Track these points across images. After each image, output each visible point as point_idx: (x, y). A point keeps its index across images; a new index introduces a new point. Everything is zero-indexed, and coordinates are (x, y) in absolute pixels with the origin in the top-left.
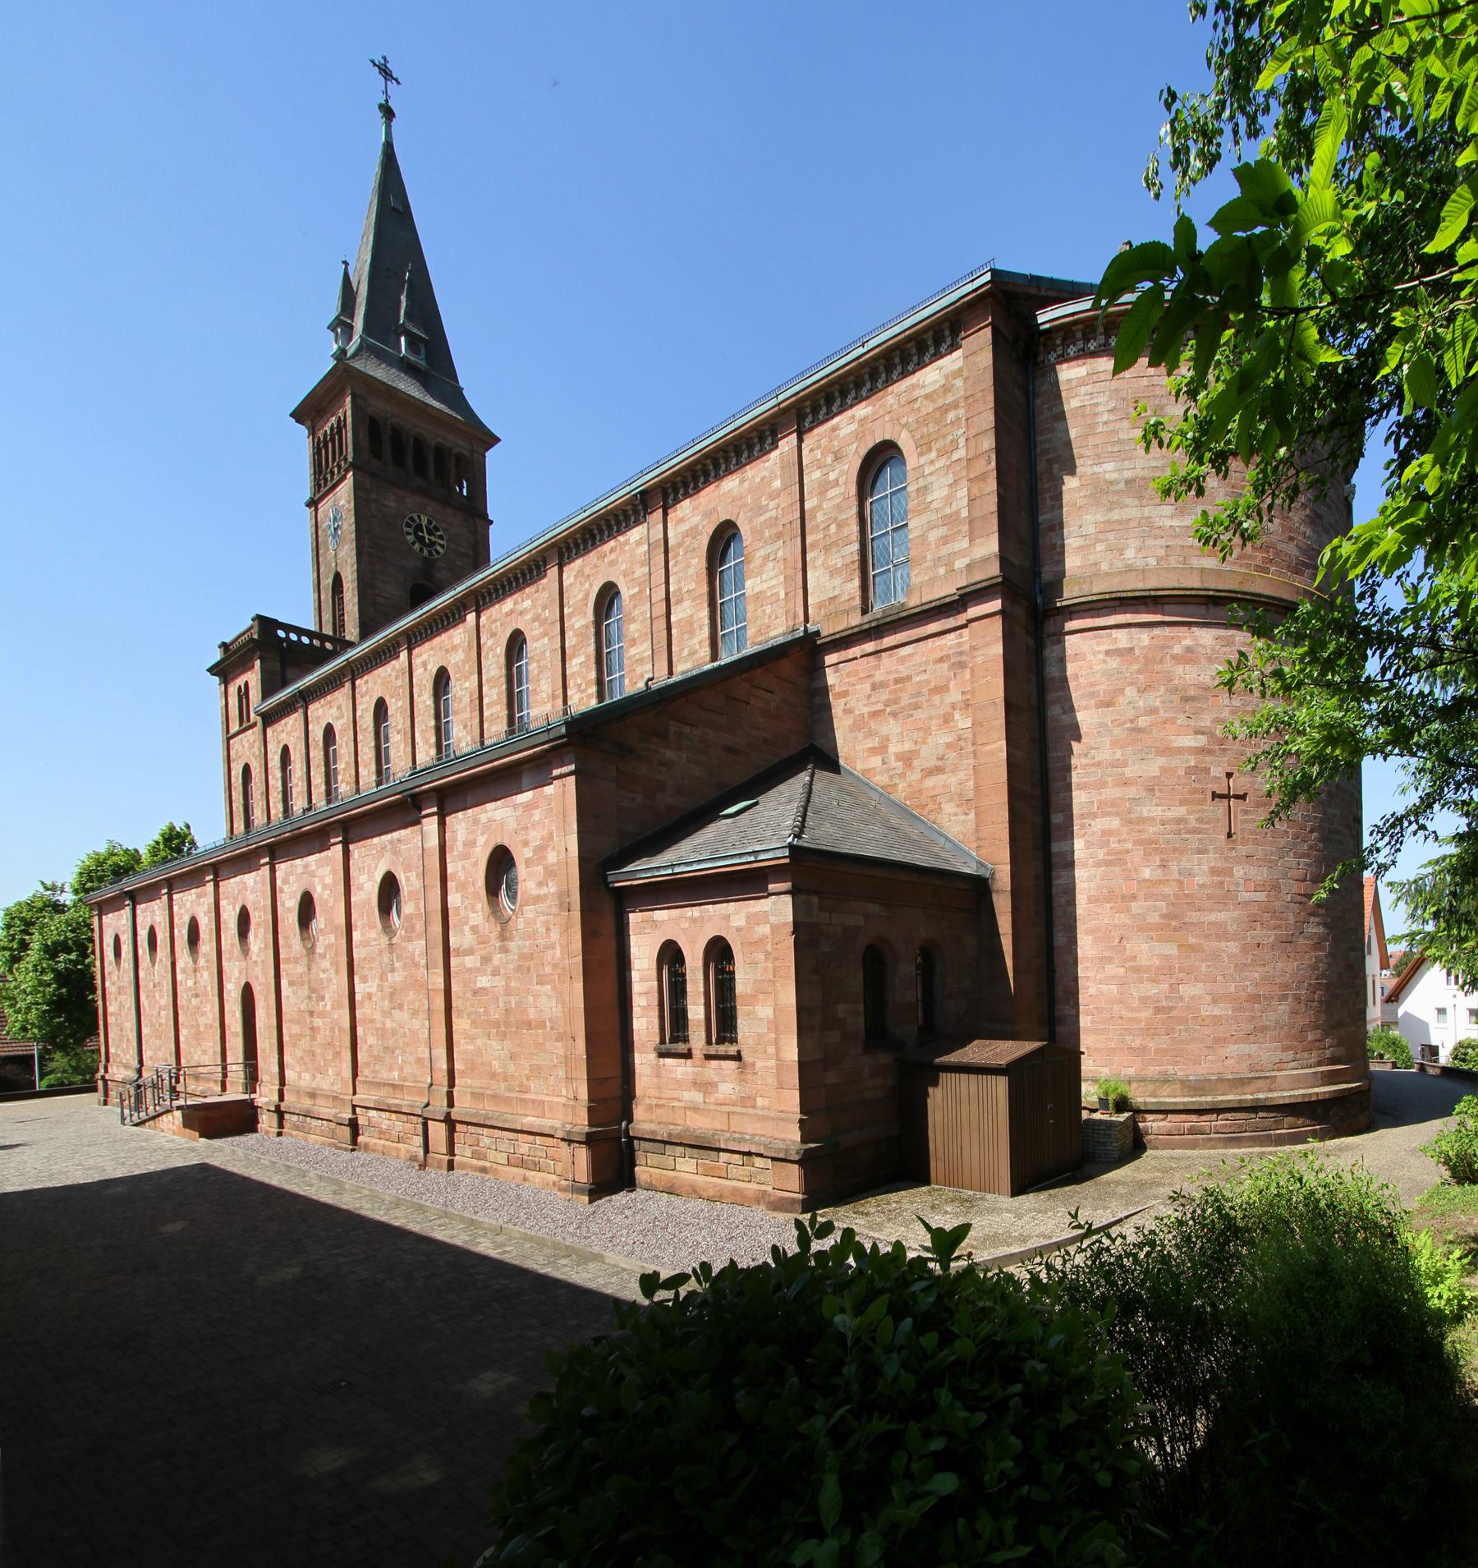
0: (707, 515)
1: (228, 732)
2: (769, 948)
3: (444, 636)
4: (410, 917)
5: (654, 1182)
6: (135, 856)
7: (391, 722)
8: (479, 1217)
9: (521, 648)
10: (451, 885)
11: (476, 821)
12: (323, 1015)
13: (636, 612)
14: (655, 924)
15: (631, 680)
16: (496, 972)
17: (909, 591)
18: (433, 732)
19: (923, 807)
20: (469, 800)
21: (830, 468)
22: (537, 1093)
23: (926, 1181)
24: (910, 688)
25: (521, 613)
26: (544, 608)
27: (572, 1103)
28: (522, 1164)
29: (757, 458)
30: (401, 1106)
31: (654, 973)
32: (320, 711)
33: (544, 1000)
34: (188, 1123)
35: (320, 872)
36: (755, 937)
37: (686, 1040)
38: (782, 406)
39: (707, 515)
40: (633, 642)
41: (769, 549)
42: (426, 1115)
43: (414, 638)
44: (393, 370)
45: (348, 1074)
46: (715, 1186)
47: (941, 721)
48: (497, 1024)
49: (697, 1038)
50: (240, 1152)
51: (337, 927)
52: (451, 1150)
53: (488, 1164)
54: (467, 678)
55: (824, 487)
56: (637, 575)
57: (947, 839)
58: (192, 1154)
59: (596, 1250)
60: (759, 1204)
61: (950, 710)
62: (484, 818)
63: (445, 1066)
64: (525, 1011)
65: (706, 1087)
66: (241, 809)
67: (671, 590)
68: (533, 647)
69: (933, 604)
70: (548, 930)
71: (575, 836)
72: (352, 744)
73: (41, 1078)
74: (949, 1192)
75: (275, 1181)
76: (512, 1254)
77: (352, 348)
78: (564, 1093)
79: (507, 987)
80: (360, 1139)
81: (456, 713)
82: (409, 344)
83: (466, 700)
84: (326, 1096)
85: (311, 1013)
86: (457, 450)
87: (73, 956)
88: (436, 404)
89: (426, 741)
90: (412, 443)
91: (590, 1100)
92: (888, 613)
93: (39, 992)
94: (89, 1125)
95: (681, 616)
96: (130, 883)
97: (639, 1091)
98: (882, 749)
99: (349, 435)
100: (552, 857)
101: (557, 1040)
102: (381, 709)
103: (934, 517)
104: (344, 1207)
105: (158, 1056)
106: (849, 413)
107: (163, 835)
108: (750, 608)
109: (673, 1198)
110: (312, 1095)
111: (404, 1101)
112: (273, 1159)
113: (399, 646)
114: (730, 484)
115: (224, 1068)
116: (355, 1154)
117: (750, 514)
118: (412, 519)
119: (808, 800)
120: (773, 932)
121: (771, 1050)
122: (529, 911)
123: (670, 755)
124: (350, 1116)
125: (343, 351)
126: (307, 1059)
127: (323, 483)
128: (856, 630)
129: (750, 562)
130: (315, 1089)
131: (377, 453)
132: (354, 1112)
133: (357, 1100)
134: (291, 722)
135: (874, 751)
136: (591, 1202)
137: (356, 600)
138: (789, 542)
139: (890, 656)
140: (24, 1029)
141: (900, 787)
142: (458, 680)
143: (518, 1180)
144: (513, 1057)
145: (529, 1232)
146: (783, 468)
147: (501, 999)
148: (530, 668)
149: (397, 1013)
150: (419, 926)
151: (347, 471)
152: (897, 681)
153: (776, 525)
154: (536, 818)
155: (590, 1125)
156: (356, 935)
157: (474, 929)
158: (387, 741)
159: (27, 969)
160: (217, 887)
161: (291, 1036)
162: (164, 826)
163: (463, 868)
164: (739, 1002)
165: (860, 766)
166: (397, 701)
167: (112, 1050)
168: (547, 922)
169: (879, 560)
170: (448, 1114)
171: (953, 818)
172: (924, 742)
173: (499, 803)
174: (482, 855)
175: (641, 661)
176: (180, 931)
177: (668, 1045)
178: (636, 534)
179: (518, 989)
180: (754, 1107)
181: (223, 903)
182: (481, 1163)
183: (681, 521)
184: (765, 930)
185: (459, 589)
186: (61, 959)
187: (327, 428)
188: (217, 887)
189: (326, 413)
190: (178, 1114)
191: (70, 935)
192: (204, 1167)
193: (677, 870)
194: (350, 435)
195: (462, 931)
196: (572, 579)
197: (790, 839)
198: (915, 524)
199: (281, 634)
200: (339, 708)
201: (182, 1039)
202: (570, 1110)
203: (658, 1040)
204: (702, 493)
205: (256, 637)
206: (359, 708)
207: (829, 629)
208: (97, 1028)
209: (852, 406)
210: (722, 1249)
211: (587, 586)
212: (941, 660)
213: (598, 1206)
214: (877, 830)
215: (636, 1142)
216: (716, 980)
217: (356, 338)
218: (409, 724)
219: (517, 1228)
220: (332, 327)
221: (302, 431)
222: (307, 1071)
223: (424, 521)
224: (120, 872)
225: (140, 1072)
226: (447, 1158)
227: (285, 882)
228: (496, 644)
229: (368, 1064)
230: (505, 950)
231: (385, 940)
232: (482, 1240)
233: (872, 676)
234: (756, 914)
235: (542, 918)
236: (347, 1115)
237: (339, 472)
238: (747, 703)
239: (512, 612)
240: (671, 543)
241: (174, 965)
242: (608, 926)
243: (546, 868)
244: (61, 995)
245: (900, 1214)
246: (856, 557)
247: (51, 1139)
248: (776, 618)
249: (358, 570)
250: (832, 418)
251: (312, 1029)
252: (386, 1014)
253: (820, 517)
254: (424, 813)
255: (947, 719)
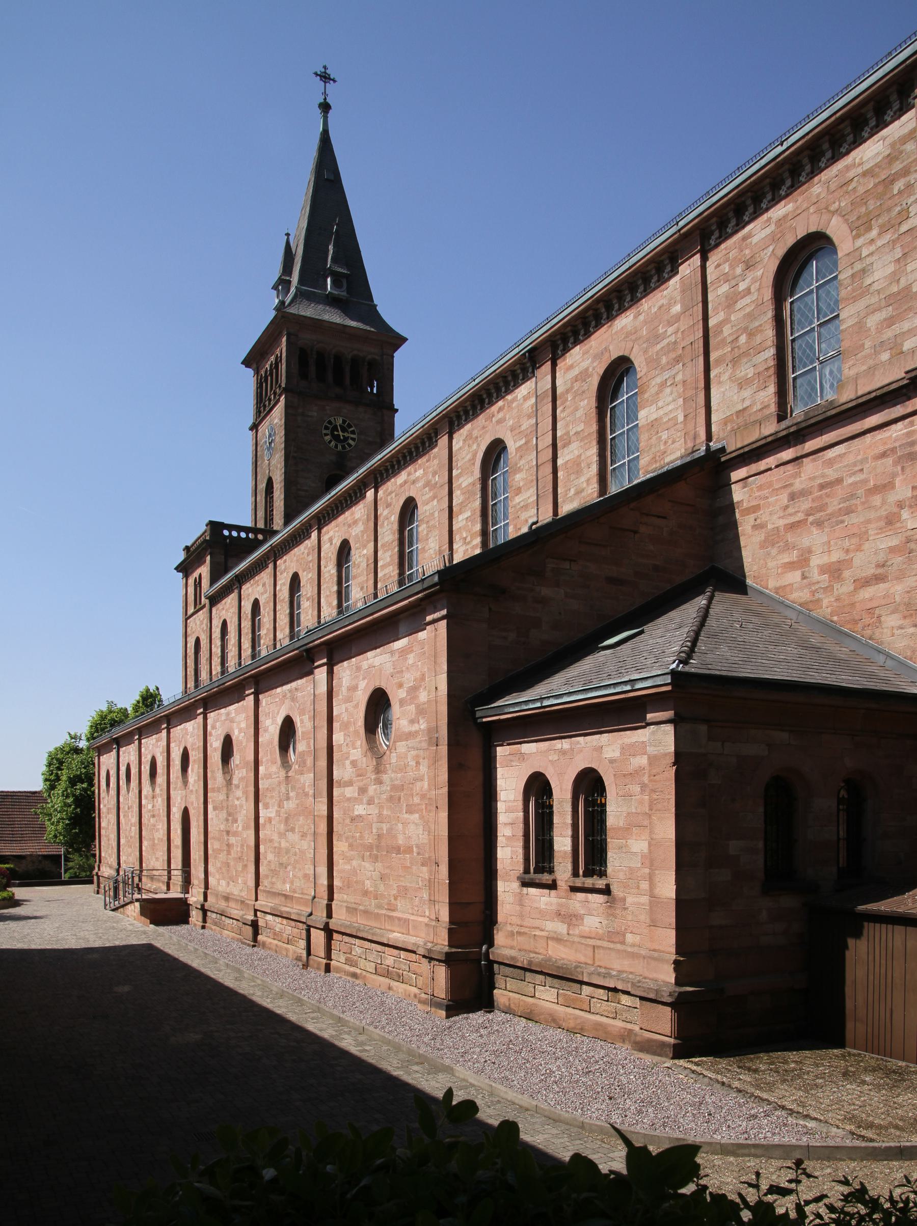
0: (596, 357)
1: (186, 614)
2: (646, 779)
3: (347, 514)
4: (302, 754)
5: (512, 1006)
6: (124, 712)
7: (303, 591)
8: (346, 1017)
9: (413, 513)
10: (336, 725)
11: (359, 669)
12: (236, 834)
13: (522, 462)
14: (522, 757)
15: (515, 526)
16: (370, 802)
17: (839, 385)
18: (335, 596)
19: (856, 622)
20: (354, 650)
21: (740, 278)
22: (403, 912)
23: (840, 1043)
24: (840, 491)
25: (414, 482)
26: (435, 473)
27: (434, 923)
28: (387, 974)
29: (654, 289)
30: (290, 913)
31: (520, 805)
32: (250, 590)
33: (412, 827)
34: (143, 912)
35: (237, 719)
36: (631, 769)
37: (551, 871)
38: (682, 232)
39: (596, 357)
40: (519, 491)
41: (666, 375)
42: (309, 923)
43: (322, 520)
44: (321, 306)
45: (252, 883)
46: (576, 1018)
47: (882, 524)
48: (370, 848)
49: (563, 869)
50: (175, 939)
51: (247, 763)
52: (328, 956)
53: (358, 971)
54: (365, 546)
55: (731, 300)
56: (523, 427)
57: (888, 656)
58: (143, 936)
59: (447, 1062)
60: (624, 1042)
61: (895, 510)
62: (365, 665)
63: (326, 883)
64: (395, 837)
65: (571, 919)
66: (193, 673)
67: (559, 434)
68: (423, 510)
69: (873, 395)
70: (418, 763)
71: (445, 676)
72: (272, 613)
73: (65, 872)
74: (871, 1059)
75: (195, 964)
76: (369, 1053)
77: (288, 300)
78: (427, 914)
79: (380, 815)
80: (260, 937)
81: (355, 577)
82: (334, 283)
83: (364, 565)
84: (237, 900)
85: (228, 833)
86: (370, 357)
87: (85, 785)
88: (354, 324)
89: (330, 604)
90: (332, 361)
91: (451, 922)
92: (811, 414)
93: (64, 811)
94: (85, 907)
95: (567, 458)
96: (117, 732)
97: (501, 917)
98: (802, 562)
99: (283, 367)
100: (423, 696)
101: (423, 865)
102: (295, 582)
103: (874, 299)
104: (241, 992)
105: (129, 860)
106: (765, 217)
107: (142, 696)
108: (643, 437)
109: (531, 1024)
110: (227, 898)
111: (293, 909)
112: (196, 947)
113: (311, 527)
114: (625, 321)
115: (169, 872)
116: (255, 949)
117: (645, 345)
118: (330, 422)
119: (702, 624)
120: (650, 764)
121: (645, 885)
122: (401, 747)
123: (545, 591)
124: (252, 918)
125: (282, 303)
126: (224, 870)
127: (262, 408)
128: (770, 439)
129: (643, 392)
130: (228, 894)
131: (304, 374)
132: (256, 915)
133: (258, 905)
134: (229, 601)
135: (791, 566)
136: (448, 1017)
137: (282, 496)
138: (689, 365)
139: (814, 460)
140: (55, 836)
141: (825, 602)
142: (357, 549)
143: (384, 989)
144: (382, 878)
145: (387, 1036)
146: (683, 291)
147: (374, 825)
148: (420, 529)
149: (290, 835)
150: (309, 761)
151: (280, 396)
152: (822, 487)
153: (674, 350)
154: (411, 661)
155: (450, 945)
156: (261, 769)
157: (354, 764)
158: (299, 608)
159: (58, 794)
160: (169, 733)
161: (213, 850)
162: (142, 688)
163: (347, 709)
164: (610, 834)
165: (772, 584)
166: (307, 573)
167: (103, 854)
168: (417, 756)
169: (801, 360)
170: (327, 924)
171: (897, 632)
172: (859, 549)
173: (378, 650)
174: (362, 698)
175: (526, 507)
176: (145, 767)
177: (532, 875)
178: (524, 390)
179: (389, 816)
180: (623, 943)
181: (172, 745)
182: (352, 969)
183: (571, 367)
184: (643, 761)
185: (361, 471)
186: (78, 787)
187: (268, 366)
188: (169, 733)
189: (267, 354)
190: (137, 904)
191: (83, 771)
192: (150, 947)
193: (546, 703)
194: (284, 366)
195: (344, 765)
196: (461, 443)
197: (674, 666)
198: (848, 314)
199: (226, 533)
200: (264, 585)
201: (144, 848)
202: (432, 930)
203: (521, 869)
204: (593, 337)
205: (208, 538)
206: (279, 583)
207: (734, 444)
208: (95, 839)
209: (767, 210)
210: (577, 1081)
211: (475, 447)
212: (884, 455)
213: (455, 1022)
214: (792, 650)
215: (496, 966)
216: (586, 812)
217: (293, 290)
218: (316, 592)
219: (377, 1031)
220: (275, 287)
221: (250, 372)
222: (224, 879)
223: (340, 421)
224: (114, 723)
225: (118, 871)
226: (325, 961)
227: (214, 727)
228: (391, 513)
229: (267, 876)
230: (379, 782)
231: (282, 773)
232: (346, 1036)
233: (791, 485)
234: (632, 745)
235: (413, 753)
236: (251, 917)
237: (275, 397)
238: (635, 532)
239: (405, 482)
240: (559, 391)
241: (140, 792)
242: (475, 757)
243: (417, 707)
244: (76, 814)
245: (799, 1076)
246: (772, 363)
247: (62, 915)
248: (673, 442)
249: (285, 473)
250: (743, 227)
251: (228, 845)
252: (282, 835)
253: (727, 331)
254: (316, 664)
255: (891, 520)
